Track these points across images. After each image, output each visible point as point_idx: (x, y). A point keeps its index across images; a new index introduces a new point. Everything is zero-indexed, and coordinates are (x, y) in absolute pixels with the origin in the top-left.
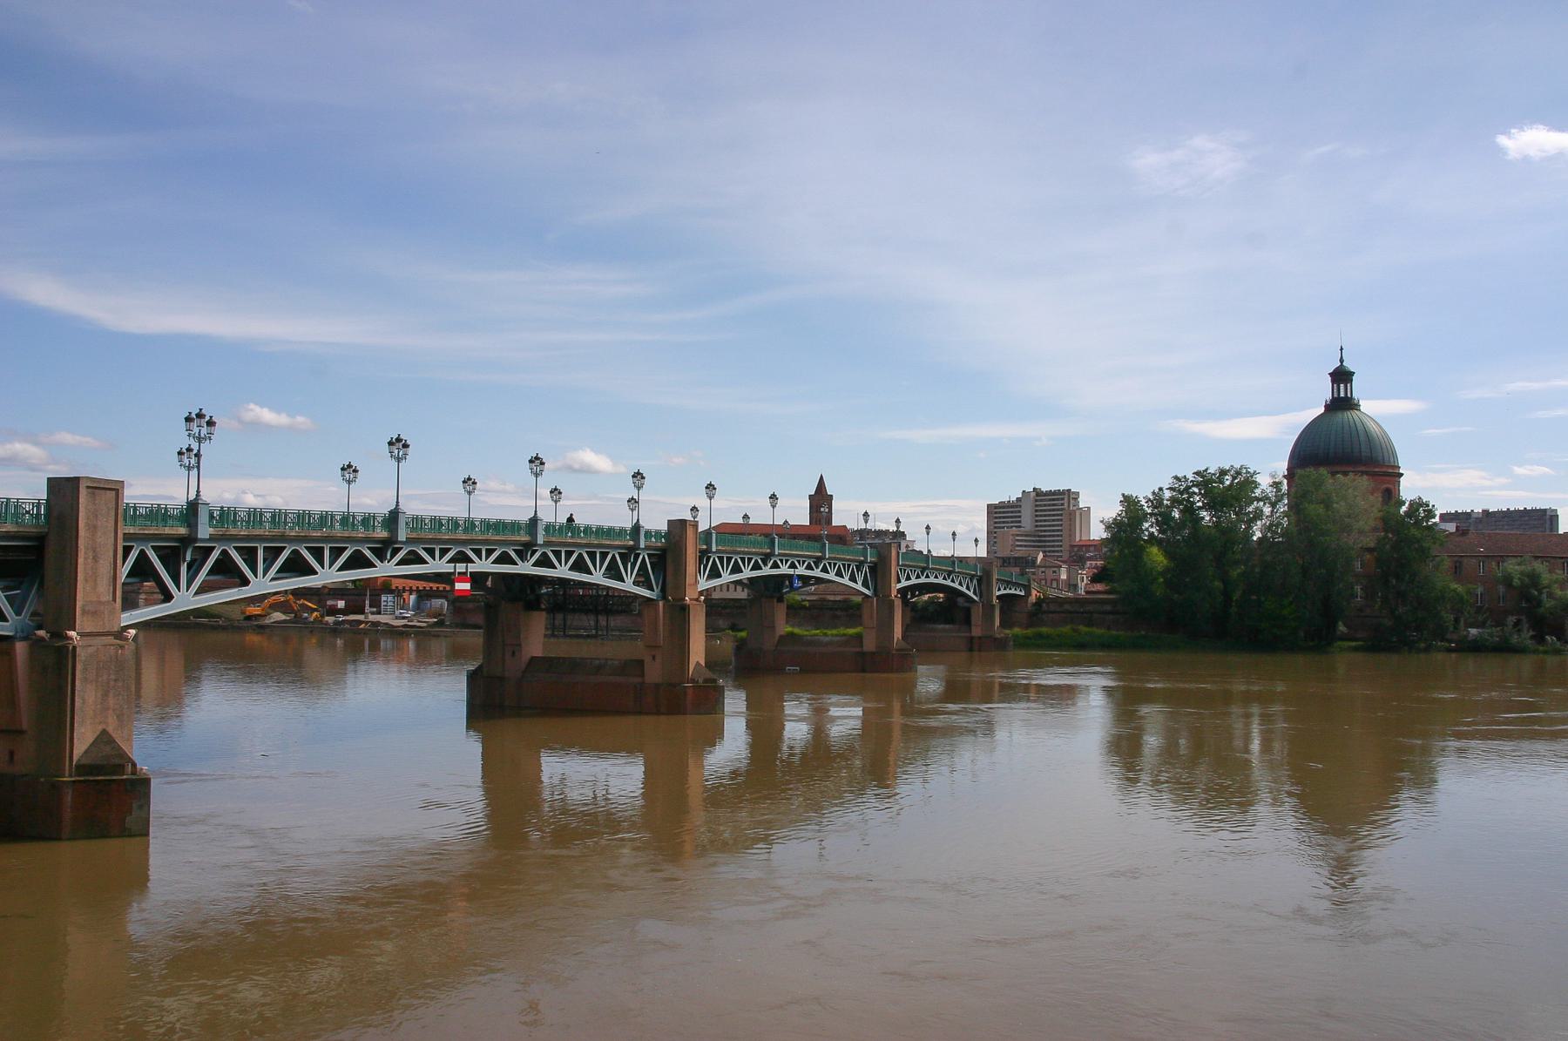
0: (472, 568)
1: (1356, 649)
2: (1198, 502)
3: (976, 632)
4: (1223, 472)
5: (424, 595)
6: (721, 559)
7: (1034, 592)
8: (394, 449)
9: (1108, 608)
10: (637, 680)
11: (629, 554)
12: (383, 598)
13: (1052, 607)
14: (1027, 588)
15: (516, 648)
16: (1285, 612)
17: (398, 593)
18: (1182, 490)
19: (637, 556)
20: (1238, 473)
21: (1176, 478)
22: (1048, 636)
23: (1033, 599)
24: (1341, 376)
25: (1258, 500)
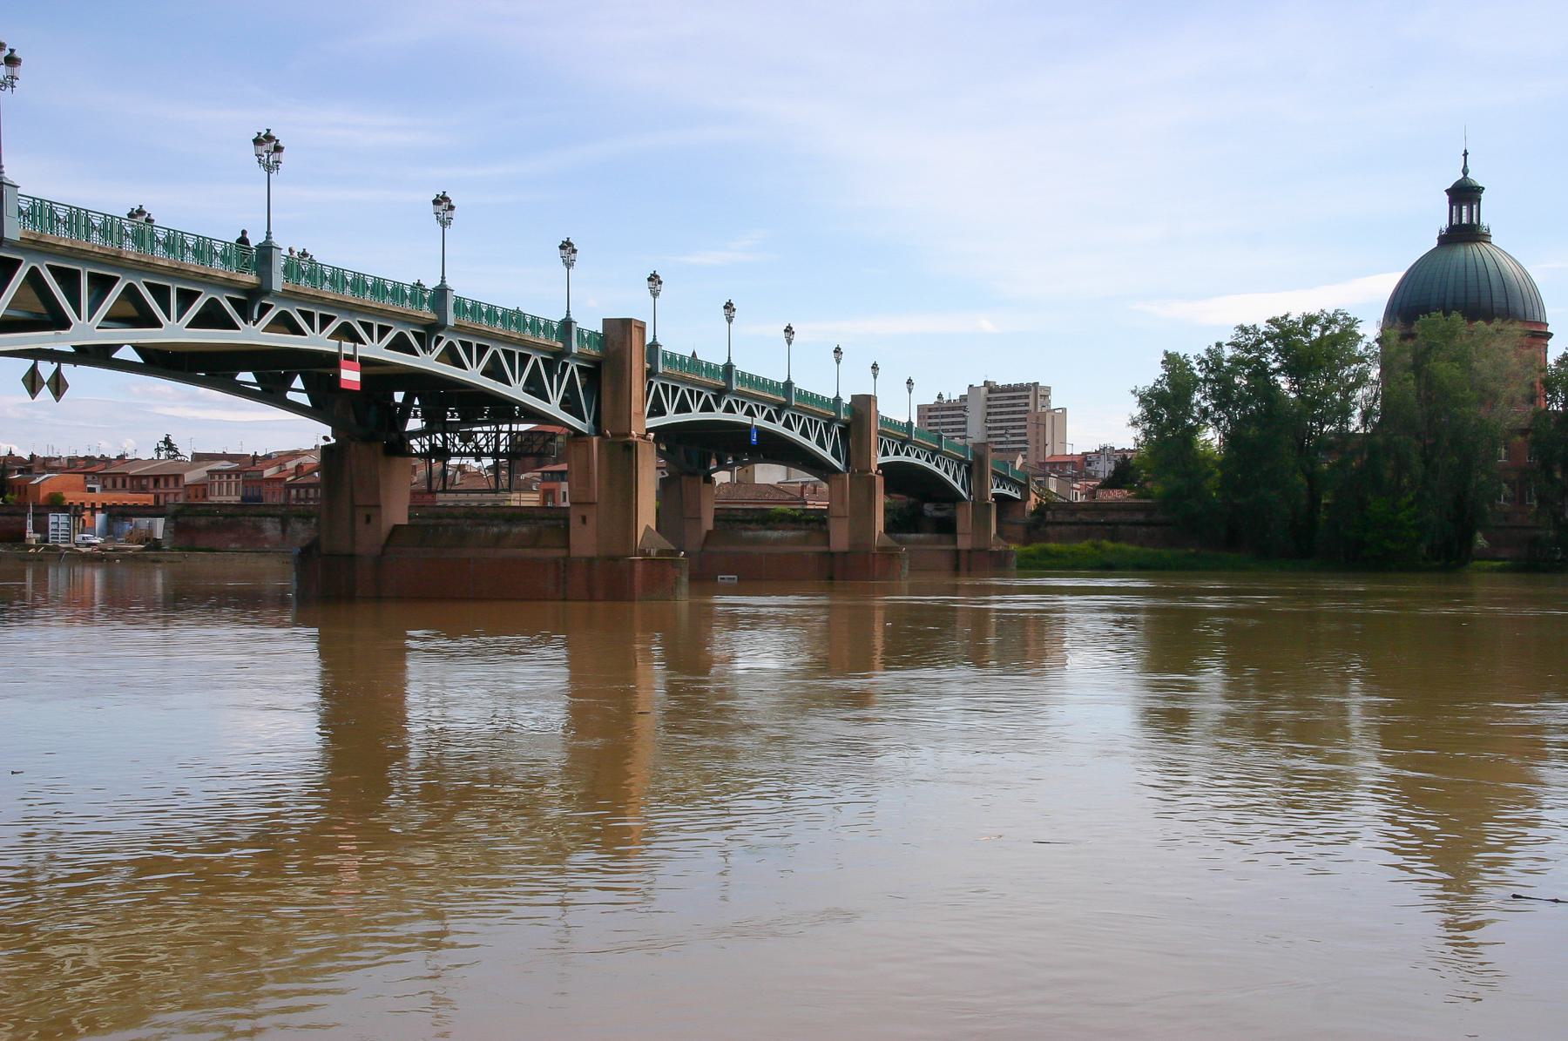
0: (364, 351)
1: (1500, 570)
2: (1273, 361)
3: (964, 543)
4: (1310, 320)
5: (117, 514)
6: (665, 387)
7: (1033, 496)
8: (261, 149)
9: (1140, 517)
10: (561, 553)
11: (555, 360)
12: (52, 518)
13: (1060, 517)
14: (1024, 488)
15: (374, 509)
16: (1401, 516)
17: (75, 511)
18: (1250, 343)
19: (565, 366)
20: (1332, 321)
21: (1244, 330)
22: (1058, 555)
23: (1032, 504)
24: (1464, 193)
25: (1361, 359)
